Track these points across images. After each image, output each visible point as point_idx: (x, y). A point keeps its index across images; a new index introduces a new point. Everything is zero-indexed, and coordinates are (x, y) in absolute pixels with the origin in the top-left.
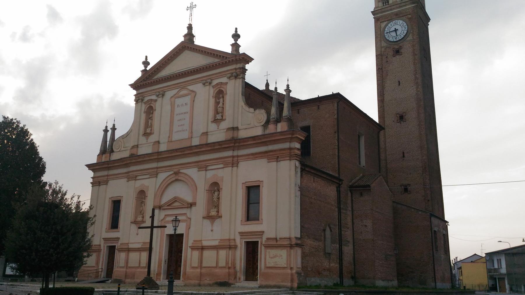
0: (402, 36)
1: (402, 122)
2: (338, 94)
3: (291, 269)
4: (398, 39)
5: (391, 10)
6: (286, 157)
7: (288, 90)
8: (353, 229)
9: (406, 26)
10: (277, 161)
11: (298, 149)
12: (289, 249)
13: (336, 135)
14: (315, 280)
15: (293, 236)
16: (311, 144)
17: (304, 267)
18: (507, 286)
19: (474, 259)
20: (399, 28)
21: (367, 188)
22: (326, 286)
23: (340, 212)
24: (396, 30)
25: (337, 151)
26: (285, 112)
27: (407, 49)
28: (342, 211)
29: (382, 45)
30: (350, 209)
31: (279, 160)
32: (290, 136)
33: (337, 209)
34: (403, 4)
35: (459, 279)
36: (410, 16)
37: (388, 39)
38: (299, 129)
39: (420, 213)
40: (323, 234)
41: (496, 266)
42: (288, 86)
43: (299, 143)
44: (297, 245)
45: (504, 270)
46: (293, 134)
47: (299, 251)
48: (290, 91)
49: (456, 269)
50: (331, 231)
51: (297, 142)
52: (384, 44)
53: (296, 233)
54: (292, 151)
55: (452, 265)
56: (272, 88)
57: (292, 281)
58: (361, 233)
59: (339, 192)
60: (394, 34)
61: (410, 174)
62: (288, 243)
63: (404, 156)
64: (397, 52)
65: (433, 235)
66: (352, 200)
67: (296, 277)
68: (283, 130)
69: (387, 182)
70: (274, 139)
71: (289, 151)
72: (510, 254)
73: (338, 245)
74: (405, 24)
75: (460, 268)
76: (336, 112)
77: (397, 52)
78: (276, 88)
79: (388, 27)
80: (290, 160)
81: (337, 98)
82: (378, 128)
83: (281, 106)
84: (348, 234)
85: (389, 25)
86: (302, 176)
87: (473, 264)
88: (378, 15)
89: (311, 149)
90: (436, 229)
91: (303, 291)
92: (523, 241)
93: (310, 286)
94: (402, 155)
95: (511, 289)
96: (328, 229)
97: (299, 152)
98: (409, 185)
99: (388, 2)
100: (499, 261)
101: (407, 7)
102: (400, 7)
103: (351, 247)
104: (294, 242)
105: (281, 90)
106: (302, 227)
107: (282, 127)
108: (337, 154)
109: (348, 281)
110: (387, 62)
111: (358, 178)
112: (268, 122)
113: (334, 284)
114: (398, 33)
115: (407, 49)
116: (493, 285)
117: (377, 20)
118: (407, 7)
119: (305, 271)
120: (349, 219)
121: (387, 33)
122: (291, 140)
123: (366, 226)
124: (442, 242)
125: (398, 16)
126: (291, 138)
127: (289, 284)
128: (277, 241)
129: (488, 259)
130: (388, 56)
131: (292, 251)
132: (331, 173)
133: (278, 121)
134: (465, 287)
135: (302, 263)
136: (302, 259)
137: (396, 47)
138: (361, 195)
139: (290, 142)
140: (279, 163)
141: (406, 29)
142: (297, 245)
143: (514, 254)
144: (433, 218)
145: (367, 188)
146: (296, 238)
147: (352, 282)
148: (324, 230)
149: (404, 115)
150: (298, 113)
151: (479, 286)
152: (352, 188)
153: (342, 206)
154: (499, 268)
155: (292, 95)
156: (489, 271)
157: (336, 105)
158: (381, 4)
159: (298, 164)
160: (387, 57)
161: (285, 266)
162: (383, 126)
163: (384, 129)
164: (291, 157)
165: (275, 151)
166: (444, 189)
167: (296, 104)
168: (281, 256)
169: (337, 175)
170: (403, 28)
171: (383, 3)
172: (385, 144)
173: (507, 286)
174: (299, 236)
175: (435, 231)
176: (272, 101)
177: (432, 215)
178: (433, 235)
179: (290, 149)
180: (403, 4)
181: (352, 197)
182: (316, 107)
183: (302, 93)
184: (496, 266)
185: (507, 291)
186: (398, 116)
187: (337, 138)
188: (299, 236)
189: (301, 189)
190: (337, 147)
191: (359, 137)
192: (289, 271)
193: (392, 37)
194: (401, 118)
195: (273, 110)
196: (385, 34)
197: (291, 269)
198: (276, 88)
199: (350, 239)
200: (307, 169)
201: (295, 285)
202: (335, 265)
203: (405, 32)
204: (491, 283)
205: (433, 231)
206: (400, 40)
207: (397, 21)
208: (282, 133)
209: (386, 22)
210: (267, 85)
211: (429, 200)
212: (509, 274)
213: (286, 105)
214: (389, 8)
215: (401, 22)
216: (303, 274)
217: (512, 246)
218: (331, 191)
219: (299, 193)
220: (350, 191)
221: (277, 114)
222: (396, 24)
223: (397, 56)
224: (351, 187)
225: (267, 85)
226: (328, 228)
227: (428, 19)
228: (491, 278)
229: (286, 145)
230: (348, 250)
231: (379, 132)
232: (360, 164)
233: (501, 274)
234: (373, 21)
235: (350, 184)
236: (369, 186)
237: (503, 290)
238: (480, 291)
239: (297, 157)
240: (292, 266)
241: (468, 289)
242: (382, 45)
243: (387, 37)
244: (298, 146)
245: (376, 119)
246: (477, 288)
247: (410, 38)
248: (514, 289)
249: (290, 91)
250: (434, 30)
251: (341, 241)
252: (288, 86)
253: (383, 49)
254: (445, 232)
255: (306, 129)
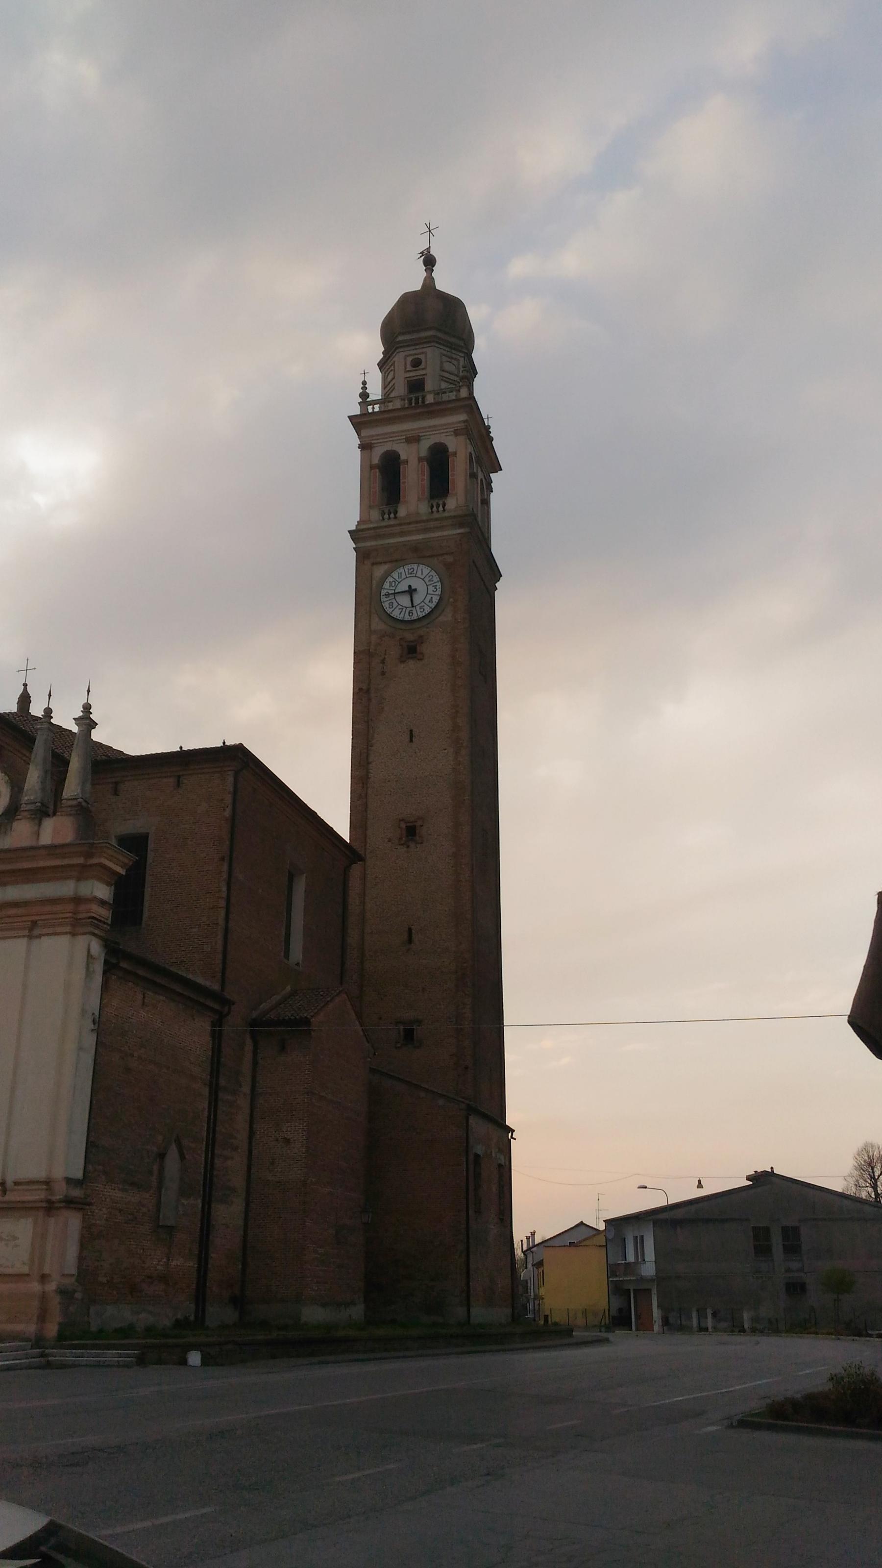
0: (427, 610)
1: (412, 844)
2: (240, 750)
3: (44, 1278)
4: (415, 617)
5: (402, 534)
6: (61, 925)
7: (87, 721)
8: (250, 1152)
9: (439, 585)
10: (30, 937)
11: (102, 903)
12: (41, 1214)
13: (225, 867)
14: (118, 1314)
15: (59, 1173)
16: (148, 891)
17: (84, 1274)
18: (656, 1313)
19: (578, 1237)
20: (419, 587)
21: (297, 1028)
22: (149, 1331)
23: (216, 1100)
24: (411, 591)
25: (222, 913)
26: (72, 787)
27: (438, 647)
28: (221, 1095)
29: (373, 627)
30: (246, 1089)
31: (36, 932)
32: (81, 860)
33: (206, 1091)
34: (432, 524)
35: (537, 1297)
36: (450, 559)
37: (389, 611)
38: (114, 842)
39: (441, 1102)
40: (155, 1168)
41: (631, 1258)
42: (87, 708)
43: (108, 884)
44: (69, 1203)
45: (649, 1269)
46: (89, 855)
47: (74, 1222)
48: (93, 725)
49: (530, 1266)
50: (182, 1157)
51: (100, 879)
52: (378, 625)
53: (69, 1163)
54: (82, 908)
55: (519, 1253)
56: (37, 710)
57: (42, 1317)
58: (273, 1163)
59: (217, 1036)
60: (405, 600)
61: (424, 990)
62: (42, 1195)
63: (410, 941)
64: (412, 651)
65: (471, 1167)
66: (255, 1063)
67: (55, 1302)
68: (59, 841)
69: (359, 1016)
70: (26, 865)
71: (70, 907)
72: (666, 1221)
73: (199, 1202)
74: (436, 579)
75: (539, 1264)
76: (229, 799)
77: (412, 651)
78: (48, 712)
79: (390, 579)
80: (73, 934)
81: (236, 761)
82: (348, 854)
83: (58, 765)
84: (232, 1167)
85: (395, 575)
86: (105, 986)
87: (573, 1250)
88: (369, 544)
89: (146, 904)
90: (479, 1149)
91: (76, 1347)
92: (700, 1185)
93: (101, 1331)
94: (405, 936)
95: (666, 1322)
96: (173, 1153)
97: (105, 913)
98: (419, 1022)
99: (396, 512)
100: (639, 1242)
101: (445, 533)
102: (427, 530)
103: (237, 1206)
104: (61, 1191)
105: (66, 718)
106: (91, 1145)
107: (56, 830)
108: (221, 922)
109: (219, 1313)
110: (383, 673)
111: (276, 998)
112: (13, 811)
113: (177, 1320)
114: (417, 599)
115: (438, 647)
116: (620, 1310)
117: (363, 557)
118: (445, 533)
119: (90, 1282)
120: (241, 1120)
121: (387, 595)
122: (82, 873)
123: (287, 1141)
124: (494, 1188)
125: (419, 553)
126: (84, 867)
127: (31, 1329)
128: (5, 1192)
129: (611, 1236)
130: (386, 655)
131: (52, 1220)
132: (200, 980)
133: (42, 813)
134: (546, 1317)
135: (81, 1258)
136: (82, 1246)
137: (410, 637)
138: (283, 1048)
139: (79, 879)
140: (36, 942)
141: (439, 592)
142: (69, 1203)
143: (675, 1223)
144: (473, 1121)
145: (297, 1028)
146: (69, 1181)
147: (230, 1315)
148: (162, 1156)
149: (419, 823)
150: (116, 793)
151: (585, 1312)
152: (259, 1028)
153: (222, 1082)
154: (637, 1262)
155: (97, 735)
156: (612, 1270)
157: (230, 779)
158: (375, 515)
159: (96, 947)
160: (383, 662)
161: (25, 1270)
162: (362, 853)
163: (360, 858)
164: (77, 926)
165: (26, 904)
166: (507, 1032)
167: (110, 765)
168: (15, 1238)
169: (216, 987)
170: (431, 588)
171: (383, 514)
172: (363, 903)
173: (656, 1313)
174: (79, 1175)
175: (477, 1156)
176: (30, 749)
177: (471, 1110)
178: (471, 1167)
179: (77, 900)
180: (432, 524)
181: (255, 1053)
182: (172, 781)
183: (134, 729)
184: (631, 1258)
185: (656, 1328)
186: (403, 825)
187: (225, 876)
188: (79, 1175)
189: (100, 1025)
190: (223, 903)
191: (291, 878)
192: (35, 1286)
193: (400, 608)
194: (411, 832)
195: (34, 777)
196: (383, 599)
197: (44, 1278)
198: (48, 712)
199: (238, 1182)
200: (124, 965)
201: (52, 1330)
202: (183, 1264)
203: (436, 599)
204: (617, 1303)
205: (471, 1157)
206: (419, 620)
207: (415, 566)
208: (52, 850)
209: (386, 567)
210: (25, 700)
211: (466, 1068)
212: (661, 1278)
213: (75, 764)
214: (397, 529)
215: (426, 570)
216: (78, 1295)
217: (673, 1201)
218: (192, 1035)
219: (90, 1040)
220: (254, 1036)
221: (43, 789)
222: (412, 574)
223: (411, 663)
224: (254, 1023)
225: (25, 700)
226: (174, 1148)
227: (496, 575)
228: (618, 1289)
229: (66, 888)
230: (228, 1214)
231: (346, 870)
232: (287, 955)
233: (642, 1279)
234: (351, 557)
235: (255, 1014)
236: (307, 1022)
237: (645, 1325)
238: (587, 1328)
239: (97, 927)
240: (47, 1270)
241: (556, 1324)
242: (373, 627)
243: (386, 605)
244: (103, 891)
245: (343, 830)
246: (580, 1321)
247: (447, 616)
248: (671, 1320)
249: (93, 725)
250: (509, 607)
251: (209, 1189)
252: (87, 708)
253: (374, 638)
254: (502, 1161)
255: (136, 844)
